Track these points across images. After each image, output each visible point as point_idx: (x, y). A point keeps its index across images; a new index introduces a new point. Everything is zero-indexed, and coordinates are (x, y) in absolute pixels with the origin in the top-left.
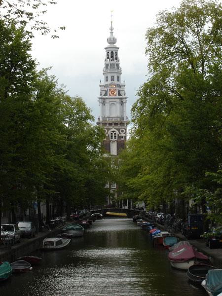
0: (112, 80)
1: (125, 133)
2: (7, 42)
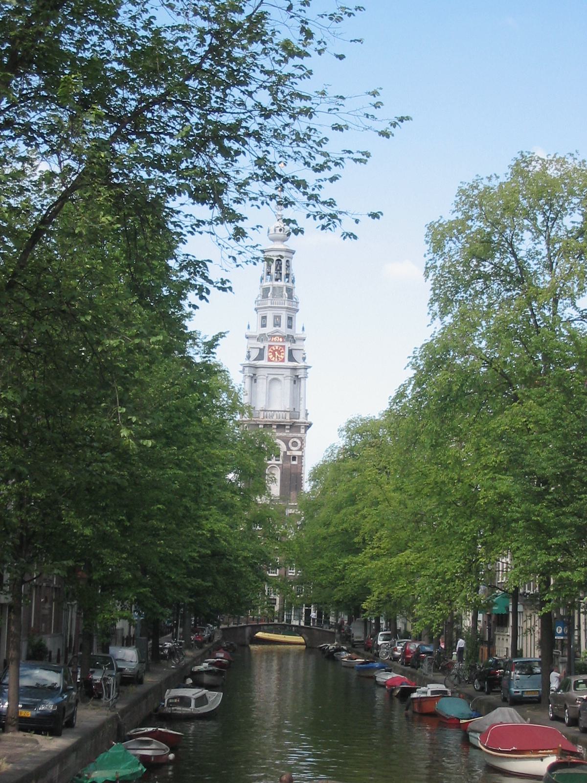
0: (275, 326)
1: (301, 449)
2: (118, 229)
